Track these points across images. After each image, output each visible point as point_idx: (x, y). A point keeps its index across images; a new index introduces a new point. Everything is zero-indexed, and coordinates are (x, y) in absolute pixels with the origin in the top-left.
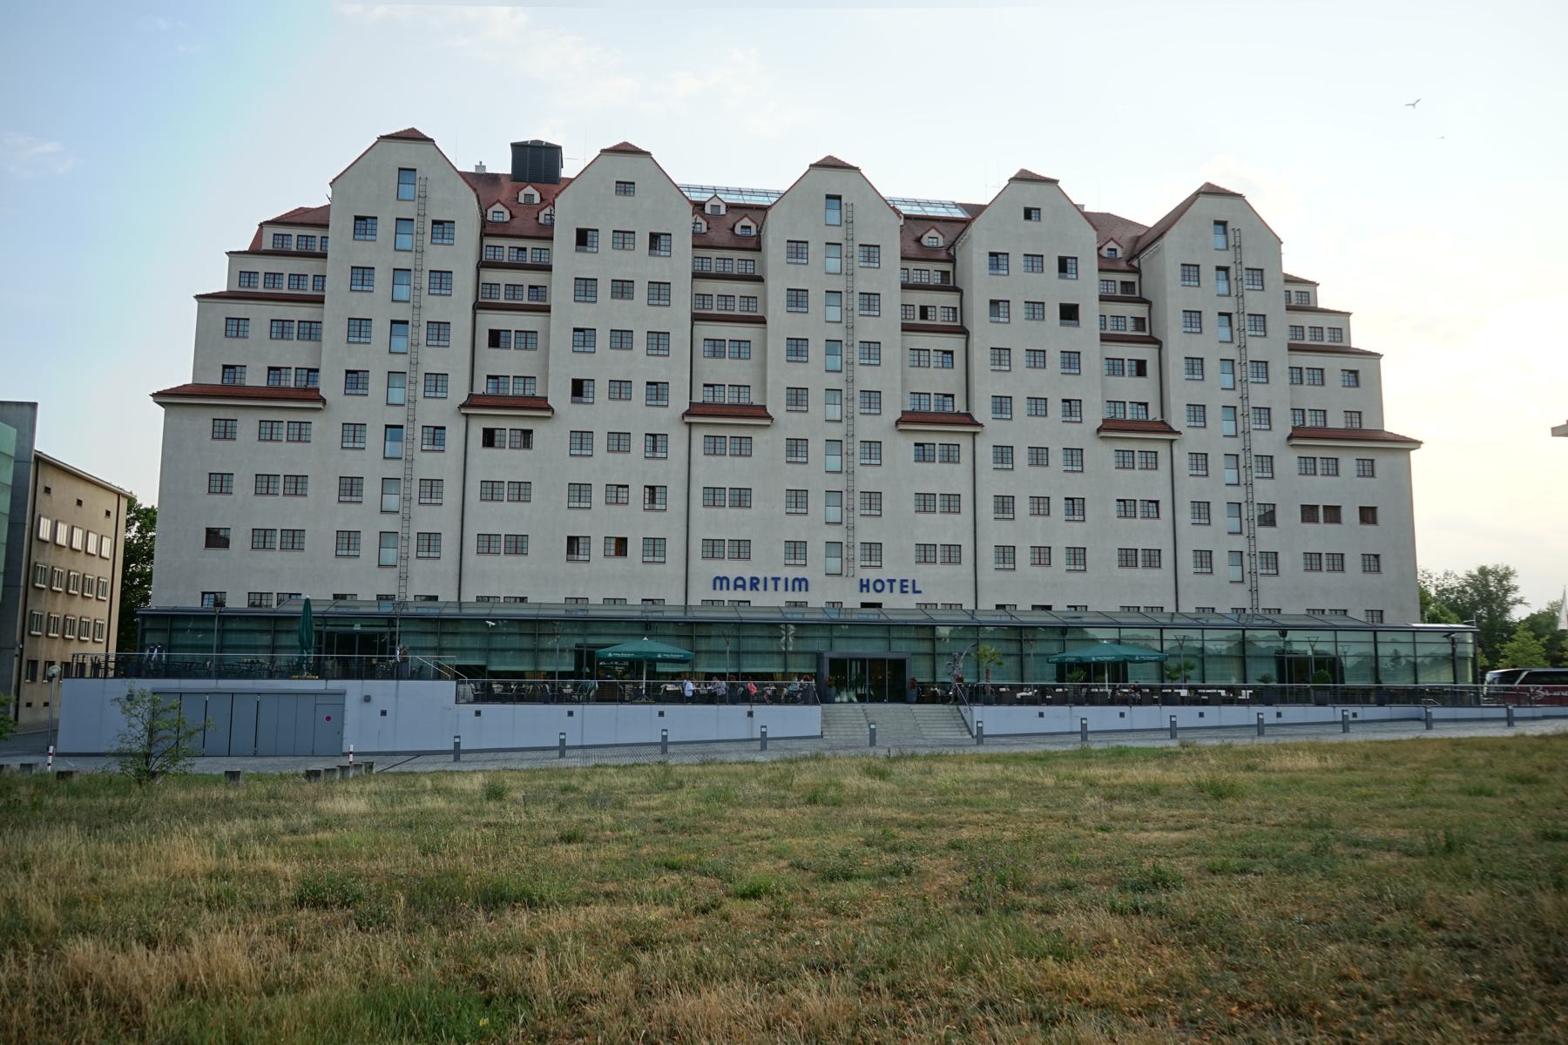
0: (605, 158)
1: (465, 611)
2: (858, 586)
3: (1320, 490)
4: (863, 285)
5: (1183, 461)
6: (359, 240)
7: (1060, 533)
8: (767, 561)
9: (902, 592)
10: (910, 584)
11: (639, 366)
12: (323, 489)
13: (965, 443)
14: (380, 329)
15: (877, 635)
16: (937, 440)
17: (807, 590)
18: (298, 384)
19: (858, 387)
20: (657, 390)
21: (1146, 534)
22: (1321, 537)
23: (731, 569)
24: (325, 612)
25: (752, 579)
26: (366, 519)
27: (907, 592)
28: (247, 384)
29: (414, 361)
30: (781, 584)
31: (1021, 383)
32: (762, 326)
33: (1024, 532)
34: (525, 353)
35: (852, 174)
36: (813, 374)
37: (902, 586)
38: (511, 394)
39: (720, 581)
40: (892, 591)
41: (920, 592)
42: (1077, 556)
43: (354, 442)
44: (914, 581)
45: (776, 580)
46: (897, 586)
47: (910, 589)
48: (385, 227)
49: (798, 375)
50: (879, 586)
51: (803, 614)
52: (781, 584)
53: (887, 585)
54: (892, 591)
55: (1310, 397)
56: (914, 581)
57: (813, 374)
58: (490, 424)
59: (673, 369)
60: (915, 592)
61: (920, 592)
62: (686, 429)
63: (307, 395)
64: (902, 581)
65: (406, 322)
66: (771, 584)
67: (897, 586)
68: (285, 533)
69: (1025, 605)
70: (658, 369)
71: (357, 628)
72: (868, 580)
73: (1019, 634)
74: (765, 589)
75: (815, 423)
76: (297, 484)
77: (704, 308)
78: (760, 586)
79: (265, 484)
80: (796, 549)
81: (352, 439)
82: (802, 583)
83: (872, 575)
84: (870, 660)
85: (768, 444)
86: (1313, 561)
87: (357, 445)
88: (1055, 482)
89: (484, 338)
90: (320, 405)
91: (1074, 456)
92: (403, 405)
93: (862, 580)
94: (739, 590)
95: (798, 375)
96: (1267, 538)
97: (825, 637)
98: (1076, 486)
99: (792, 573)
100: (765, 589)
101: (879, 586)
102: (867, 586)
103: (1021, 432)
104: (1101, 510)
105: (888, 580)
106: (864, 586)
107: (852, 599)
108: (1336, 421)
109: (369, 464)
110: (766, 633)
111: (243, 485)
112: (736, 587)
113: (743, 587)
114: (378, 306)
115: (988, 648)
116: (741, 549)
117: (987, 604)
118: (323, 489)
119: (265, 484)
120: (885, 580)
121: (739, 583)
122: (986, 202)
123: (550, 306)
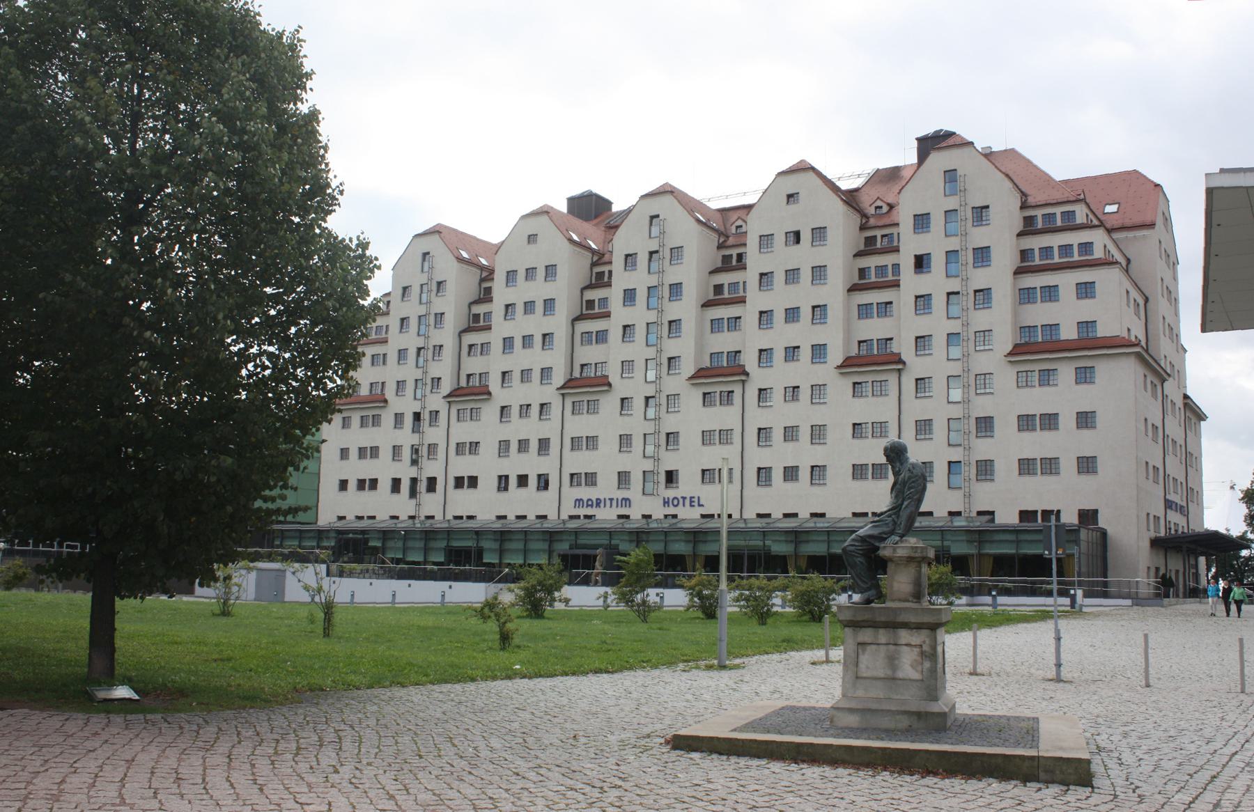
0: (778, 178)
1: (749, 525)
2: (662, 502)
3: (1038, 400)
4: (671, 278)
5: (752, 393)
6: (764, 253)
7: (804, 454)
8: (606, 487)
9: (691, 506)
10: (696, 500)
11: (803, 334)
12: (609, 444)
13: (737, 389)
14: (939, 302)
15: (960, 538)
16: (718, 389)
17: (630, 506)
18: (1045, 338)
19: (972, 329)
20: (819, 351)
21: (1038, 444)
22: (1038, 444)
23: (585, 493)
24: (942, 527)
25: (597, 499)
26: (635, 464)
27: (694, 506)
28: (1062, 338)
29: (965, 323)
30: (614, 503)
31: (781, 336)
32: (743, 304)
33: (778, 455)
34: (886, 319)
35: (966, 150)
36: (637, 350)
37: (691, 502)
38: (1040, 340)
39: (579, 502)
40: (684, 505)
41: (702, 505)
42: (817, 472)
43: (985, 388)
44: (699, 498)
45: (611, 500)
46: (687, 502)
47: (696, 504)
48: (937, 221)
49: (922, 325)
50: (675, 502)
51: (815, 523)
52: (614, 503)
53: (681, 501)
54: (684, 505)
55: (1039, 314)
56: (699, 498)
57: (937, 324)
58: (364, 413)
59: (556, 359)
60: (700, 505)
61: (702, 505)
62: (561, 397)
63: (1025, 349)
64: (691, 498)
65: (958, 293)
66: (608, 503)
67: (687, 502)
68: (1044, 461)
69: (804, 514)
70: (820, 335)
71: (351, 535)
72: (668, 498)
73: (429, 535)
74: (605, 506)
75: (935, 364)
76: (1026, 423)
77: (1027, 371)
78: (602, 505)
79: (1050, 421)
80: (623, 478)
81: (983, 386)
82: (626, 502)
83: (671, 493)
84: (456, 551)
85: (609, 404)
86: (1026, 467)
87: (988, 391)
88: (802, 414)
89: (465, 350)
90: (606, 388)
91: (818, 390)
92: (959, 359)
93: (664, 499)
94: (589, 508)
95: (922, 325)
96: (983, 449)
97: (963, 541)
98: (818, 415)
99: (621, 494)
100: (605, 506)
101: (676, 502)
102: (668, 502)
103: (515, 395)
104: (839, 433)
105: (682, 497)
106: (666, 503)
107: (658, 512)
108: (1068, 332)
109: (635, 424)
110: (783, 538)
111: (1067, 421)
112: (588, 506)
113: (592, 506)
114: (936, 282)
115: (533, 545)
116: (591, 479)
117: (750, 514)
118: (488, 449)
119: (1050, 421)
120: (679, 497)
121: (590, 504)
122: (754, 201)
123: (610, 312)
